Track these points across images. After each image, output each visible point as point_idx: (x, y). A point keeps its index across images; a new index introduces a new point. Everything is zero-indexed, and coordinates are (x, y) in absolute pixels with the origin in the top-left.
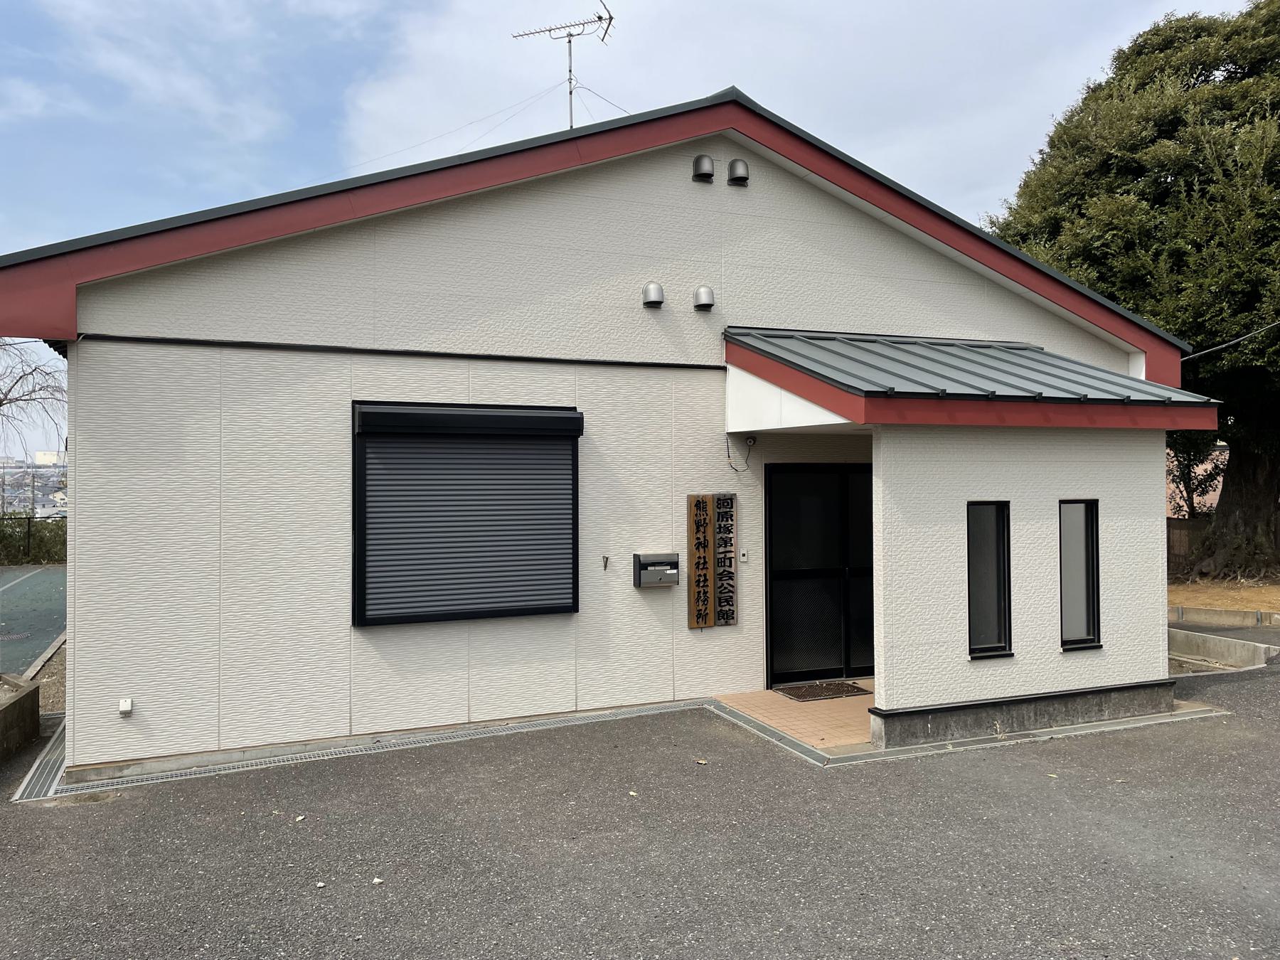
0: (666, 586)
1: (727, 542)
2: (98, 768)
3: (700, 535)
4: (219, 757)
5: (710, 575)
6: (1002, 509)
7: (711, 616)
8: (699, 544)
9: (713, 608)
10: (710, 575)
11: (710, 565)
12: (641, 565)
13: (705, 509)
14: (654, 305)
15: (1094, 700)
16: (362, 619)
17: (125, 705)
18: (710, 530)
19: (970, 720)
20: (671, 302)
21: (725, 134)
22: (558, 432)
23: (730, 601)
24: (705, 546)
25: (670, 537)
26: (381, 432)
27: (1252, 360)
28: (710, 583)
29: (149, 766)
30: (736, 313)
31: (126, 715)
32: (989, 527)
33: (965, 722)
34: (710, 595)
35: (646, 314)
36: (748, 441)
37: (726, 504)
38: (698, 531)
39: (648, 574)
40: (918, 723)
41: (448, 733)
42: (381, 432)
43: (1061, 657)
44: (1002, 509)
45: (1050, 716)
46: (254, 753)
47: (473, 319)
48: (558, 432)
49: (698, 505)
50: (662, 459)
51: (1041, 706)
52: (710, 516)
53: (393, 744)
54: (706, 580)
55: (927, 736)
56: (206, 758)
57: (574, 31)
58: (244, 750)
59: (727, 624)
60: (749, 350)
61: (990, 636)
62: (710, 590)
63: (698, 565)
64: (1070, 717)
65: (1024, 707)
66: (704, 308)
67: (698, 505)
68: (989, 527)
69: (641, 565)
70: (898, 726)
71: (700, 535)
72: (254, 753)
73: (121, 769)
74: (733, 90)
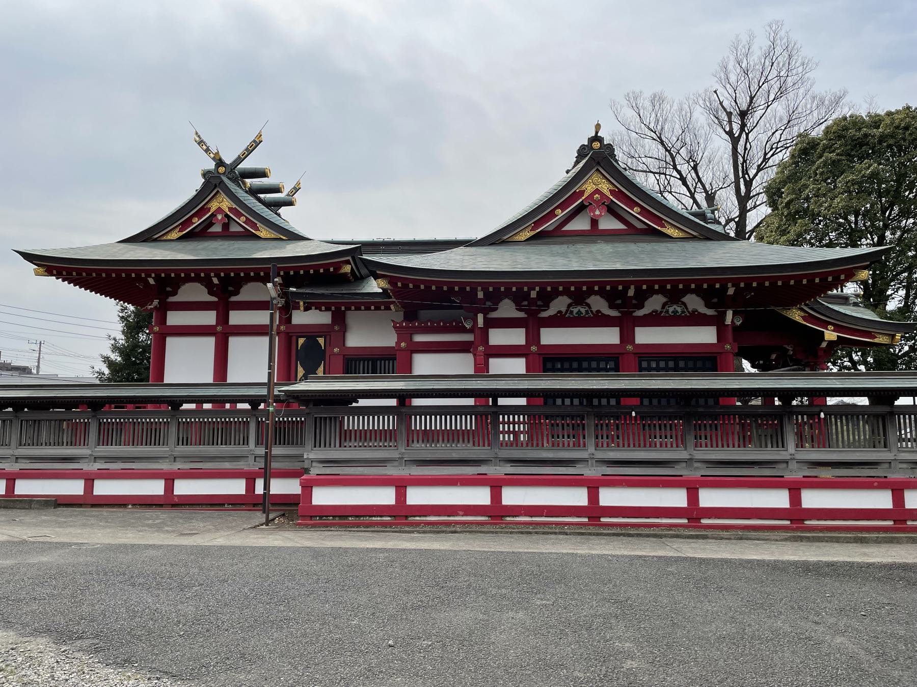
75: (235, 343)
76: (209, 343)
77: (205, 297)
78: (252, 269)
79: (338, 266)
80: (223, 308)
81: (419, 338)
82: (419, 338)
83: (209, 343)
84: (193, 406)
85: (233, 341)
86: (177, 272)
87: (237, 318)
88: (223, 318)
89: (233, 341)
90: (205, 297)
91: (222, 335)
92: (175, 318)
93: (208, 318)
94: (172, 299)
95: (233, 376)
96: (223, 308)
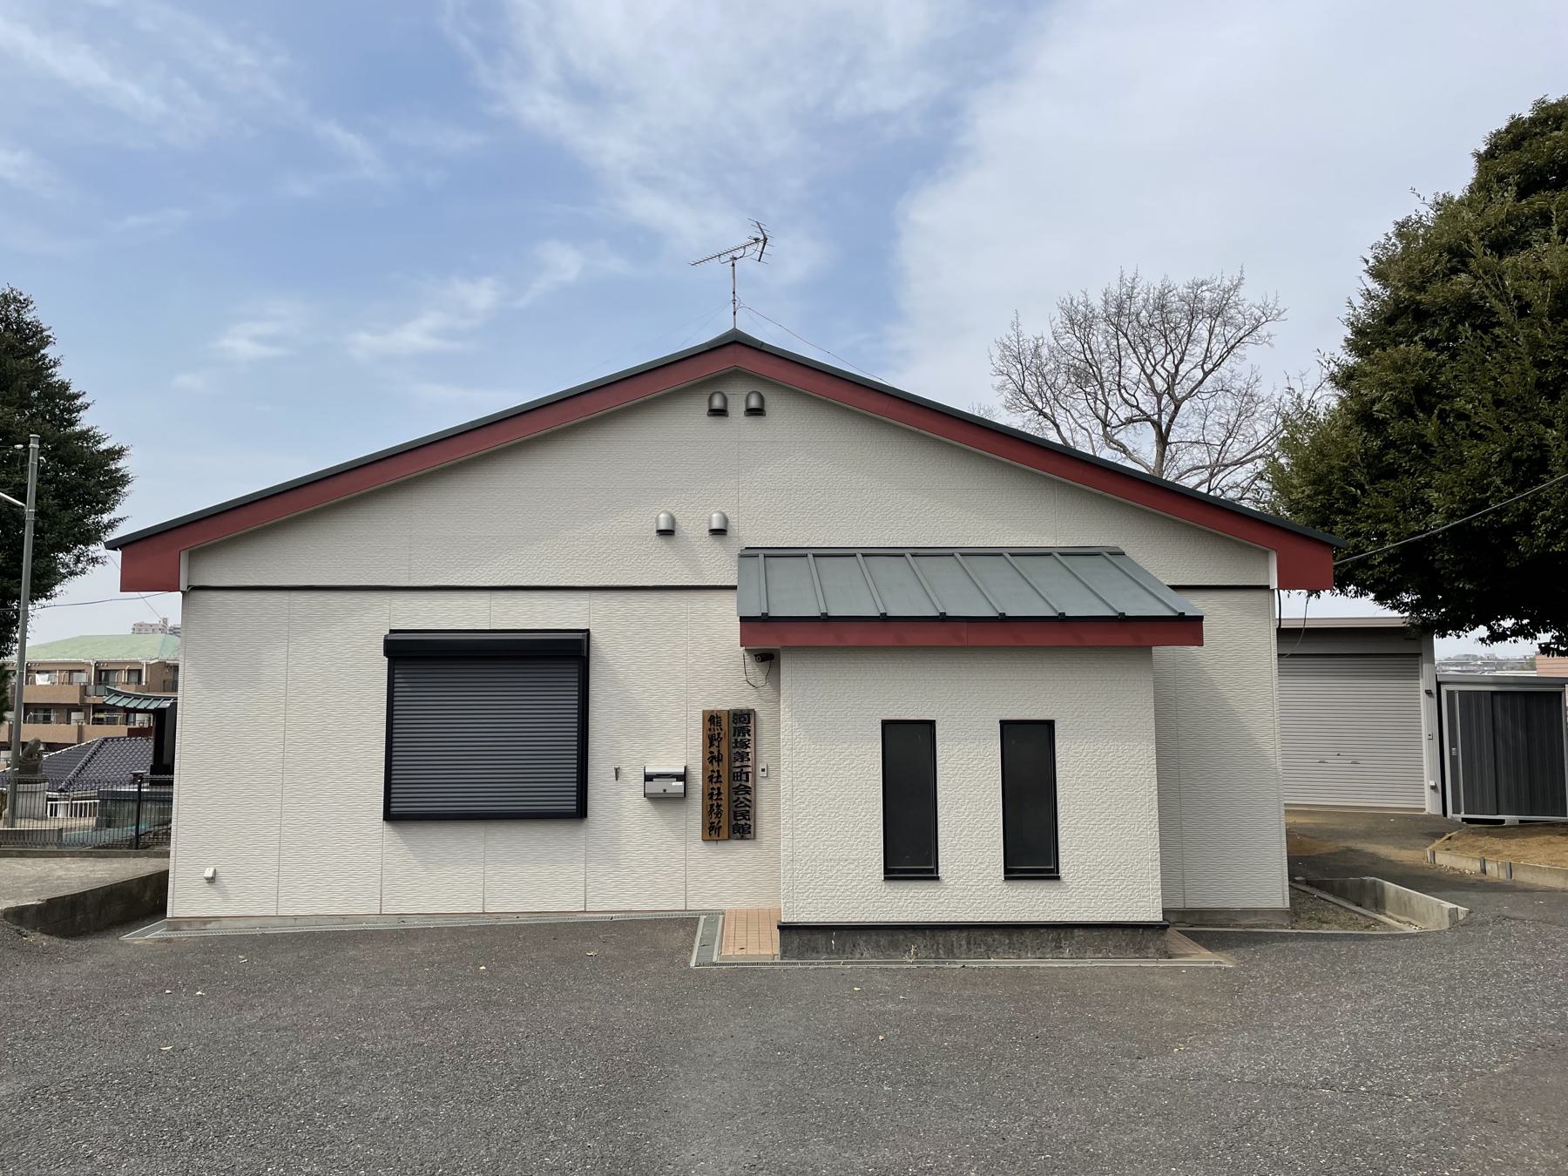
1: (743, 757)
2: (190, 921)
3: (714, 749)
4: (277, 922)
5: (724, 790)
6: (1046, 729)
7: (725, 829)
8: (712, 758)
10: (724, 790)
11: (725, 778)
13: (719, 724)
14: (666, 533)
15: (1052, 935)
16: (389, 817)
17: (209, 873)
18: (724, 744)
19: (883, 942)
20: (683, 526)
21: (733, 372)
22: (569, 655)
23: (746, 815)
24: (719, 760)
25: (682, 752)
26: (408, 655)
27: (1550, 545)
28: (724, 796)
29: (225, 922)
30: (752, 533)
31: (211, 880)
33: (877, 943)
34: (724, 809)
35: (661, 542)
38: (711, 745)
39: (663, 793)
40: (820, 939)
42: (408, 655)
43: (1004, 885)
44: (1046, 729)
45: (989, 947)
46: (303, 921)
47: (484, 562)
48: (569, 655)
49: (712, 719)
51: (977, 934)
53: (416, 924)
54: (719, 794)
55: (830, 952)
56: (267, 921)
57: (737, 254)
58: (296, 917)
59: (742, 838)
62: (724, 803)
63: (711, 778)
64: (1016, 950)
65: (954, 935)
66: (718, 532)
67: (712, 719)
70: (796, 940)
71: (714, 749)
72: (303, 921)
73: (205, 923)
74: (735, 332)
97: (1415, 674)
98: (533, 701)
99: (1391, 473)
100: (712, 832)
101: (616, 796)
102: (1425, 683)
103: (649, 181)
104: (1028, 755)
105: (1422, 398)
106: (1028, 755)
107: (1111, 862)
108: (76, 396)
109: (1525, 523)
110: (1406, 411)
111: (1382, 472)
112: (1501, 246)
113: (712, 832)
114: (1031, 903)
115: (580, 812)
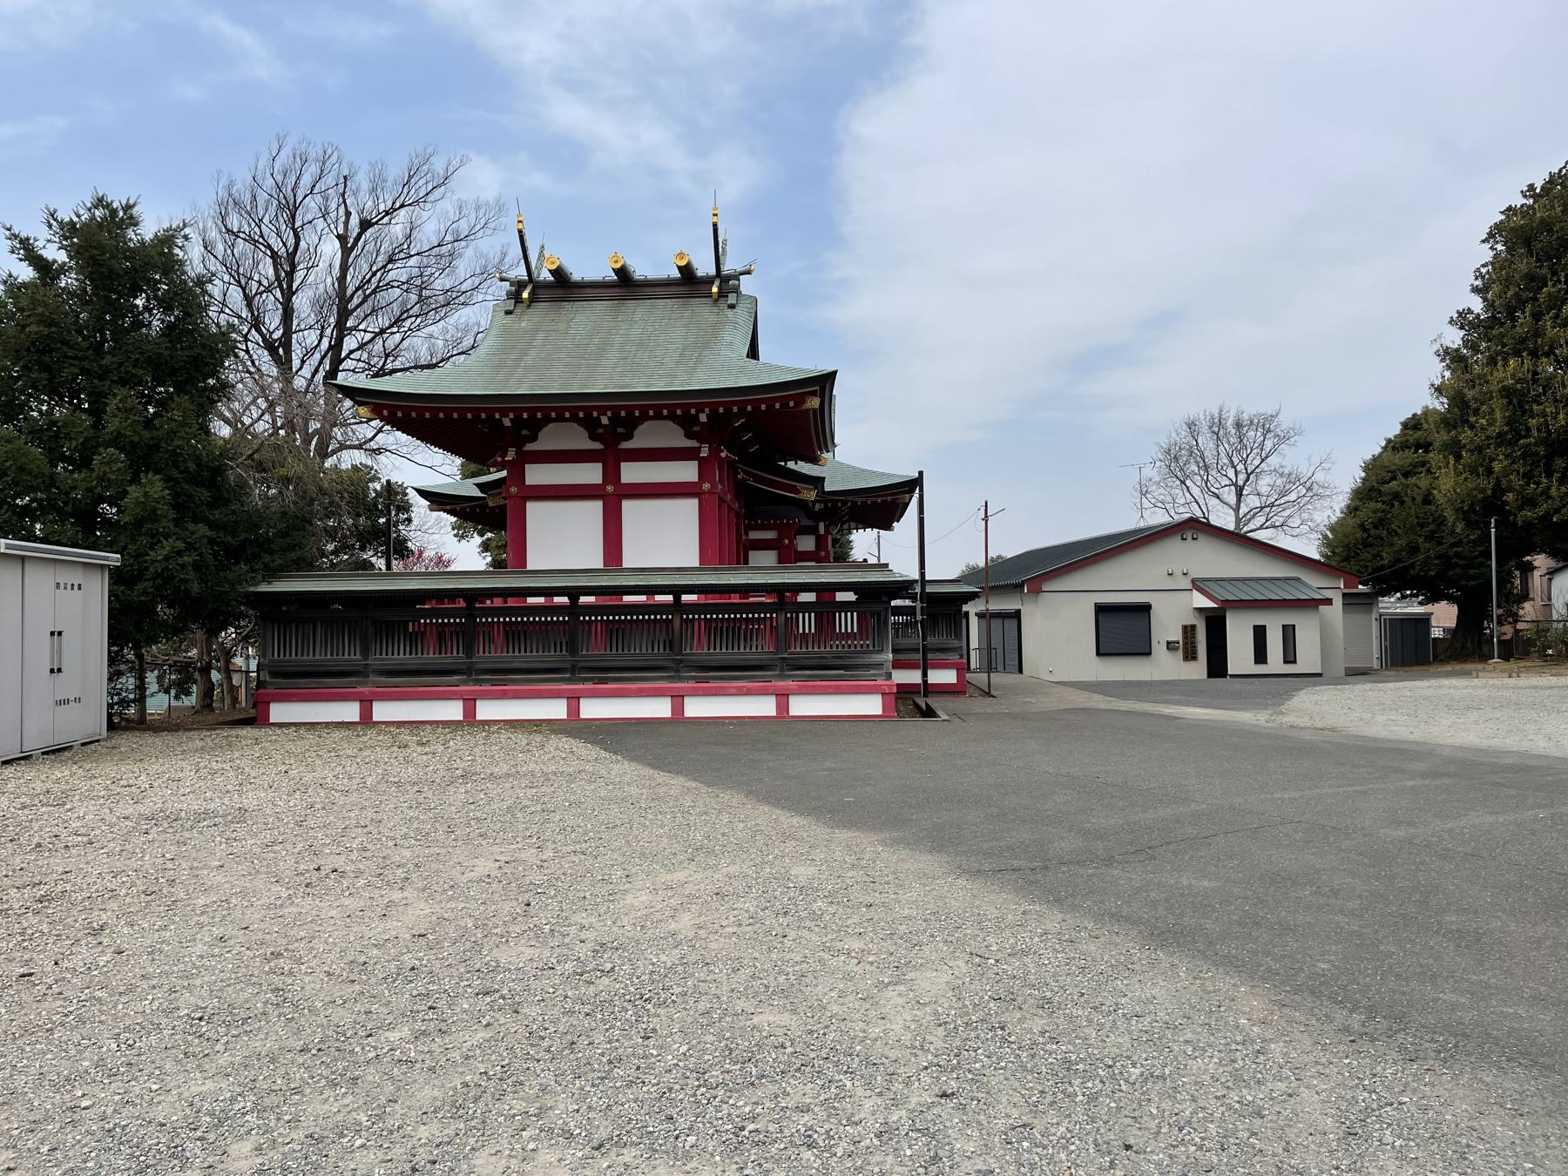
0: (1176, 649)
8: (1185, 637)
9: (1190, 655)
12: (1168, 643)
16: (1098, 654)
22: (1145, 609)
25: (1177, 636)
26: (1101, 610)
32: (1260, 633)
36: (1200, 610)
37: (1193, 627)
39: (1171, 646)
41: (318, 655)
42: (1101, 610)
47: (1121, 581)
48: (1145, 609)
49: (1185, 628)
50: (1173, 615)
52: (1189, 631)
60: (1198, 585)
61: (1261, 655)
63: (1185, 644)
67: (1185, 628)
68: (1260, 633)
69: (1168, 643)
75: (631, 510)
76: (595, 508)
77: (584, 443)
78: (623, 407)
79: (800, 399)
80: (611, 459)
81: (755, 535)
82: (755, 535)
83: (595, 508)
84: (541, 600)
85: (628, 506)
86: (532, 411)
87: (632, 473)
88: (612, 474)
89: (628, 506)
90: (584, 443)
91: (612, 497)
92: (537, 475)
93: (591, 474)
94: (530, 447)
95: (632, 557)
96: (611, 459)
97: (1370, 612)
98: (1011, 624)
99: (1371, 546)
100: (1186, 658)
101: (1159, 649)
102: (1375, 615)
103: (573, 84)
104: (1289, 633)
105: (1381, 523)
106: (1289, 633)
107: (1309, 657)
108: (884, 504)
109: (1412, 566)
110: (1376, 527)
111: (1367, 545)
112: (1406, 475)
113: (1186, 658)
114: (1290, 669)
115: (1150, 654)
